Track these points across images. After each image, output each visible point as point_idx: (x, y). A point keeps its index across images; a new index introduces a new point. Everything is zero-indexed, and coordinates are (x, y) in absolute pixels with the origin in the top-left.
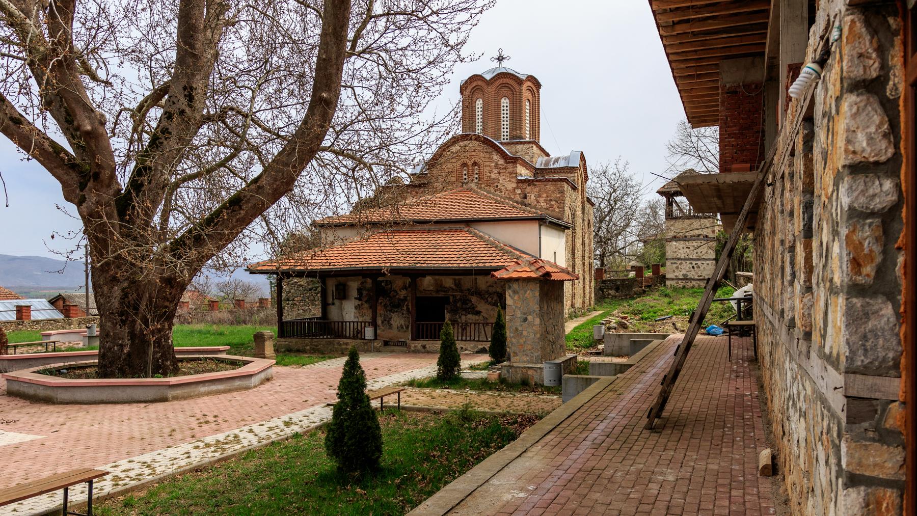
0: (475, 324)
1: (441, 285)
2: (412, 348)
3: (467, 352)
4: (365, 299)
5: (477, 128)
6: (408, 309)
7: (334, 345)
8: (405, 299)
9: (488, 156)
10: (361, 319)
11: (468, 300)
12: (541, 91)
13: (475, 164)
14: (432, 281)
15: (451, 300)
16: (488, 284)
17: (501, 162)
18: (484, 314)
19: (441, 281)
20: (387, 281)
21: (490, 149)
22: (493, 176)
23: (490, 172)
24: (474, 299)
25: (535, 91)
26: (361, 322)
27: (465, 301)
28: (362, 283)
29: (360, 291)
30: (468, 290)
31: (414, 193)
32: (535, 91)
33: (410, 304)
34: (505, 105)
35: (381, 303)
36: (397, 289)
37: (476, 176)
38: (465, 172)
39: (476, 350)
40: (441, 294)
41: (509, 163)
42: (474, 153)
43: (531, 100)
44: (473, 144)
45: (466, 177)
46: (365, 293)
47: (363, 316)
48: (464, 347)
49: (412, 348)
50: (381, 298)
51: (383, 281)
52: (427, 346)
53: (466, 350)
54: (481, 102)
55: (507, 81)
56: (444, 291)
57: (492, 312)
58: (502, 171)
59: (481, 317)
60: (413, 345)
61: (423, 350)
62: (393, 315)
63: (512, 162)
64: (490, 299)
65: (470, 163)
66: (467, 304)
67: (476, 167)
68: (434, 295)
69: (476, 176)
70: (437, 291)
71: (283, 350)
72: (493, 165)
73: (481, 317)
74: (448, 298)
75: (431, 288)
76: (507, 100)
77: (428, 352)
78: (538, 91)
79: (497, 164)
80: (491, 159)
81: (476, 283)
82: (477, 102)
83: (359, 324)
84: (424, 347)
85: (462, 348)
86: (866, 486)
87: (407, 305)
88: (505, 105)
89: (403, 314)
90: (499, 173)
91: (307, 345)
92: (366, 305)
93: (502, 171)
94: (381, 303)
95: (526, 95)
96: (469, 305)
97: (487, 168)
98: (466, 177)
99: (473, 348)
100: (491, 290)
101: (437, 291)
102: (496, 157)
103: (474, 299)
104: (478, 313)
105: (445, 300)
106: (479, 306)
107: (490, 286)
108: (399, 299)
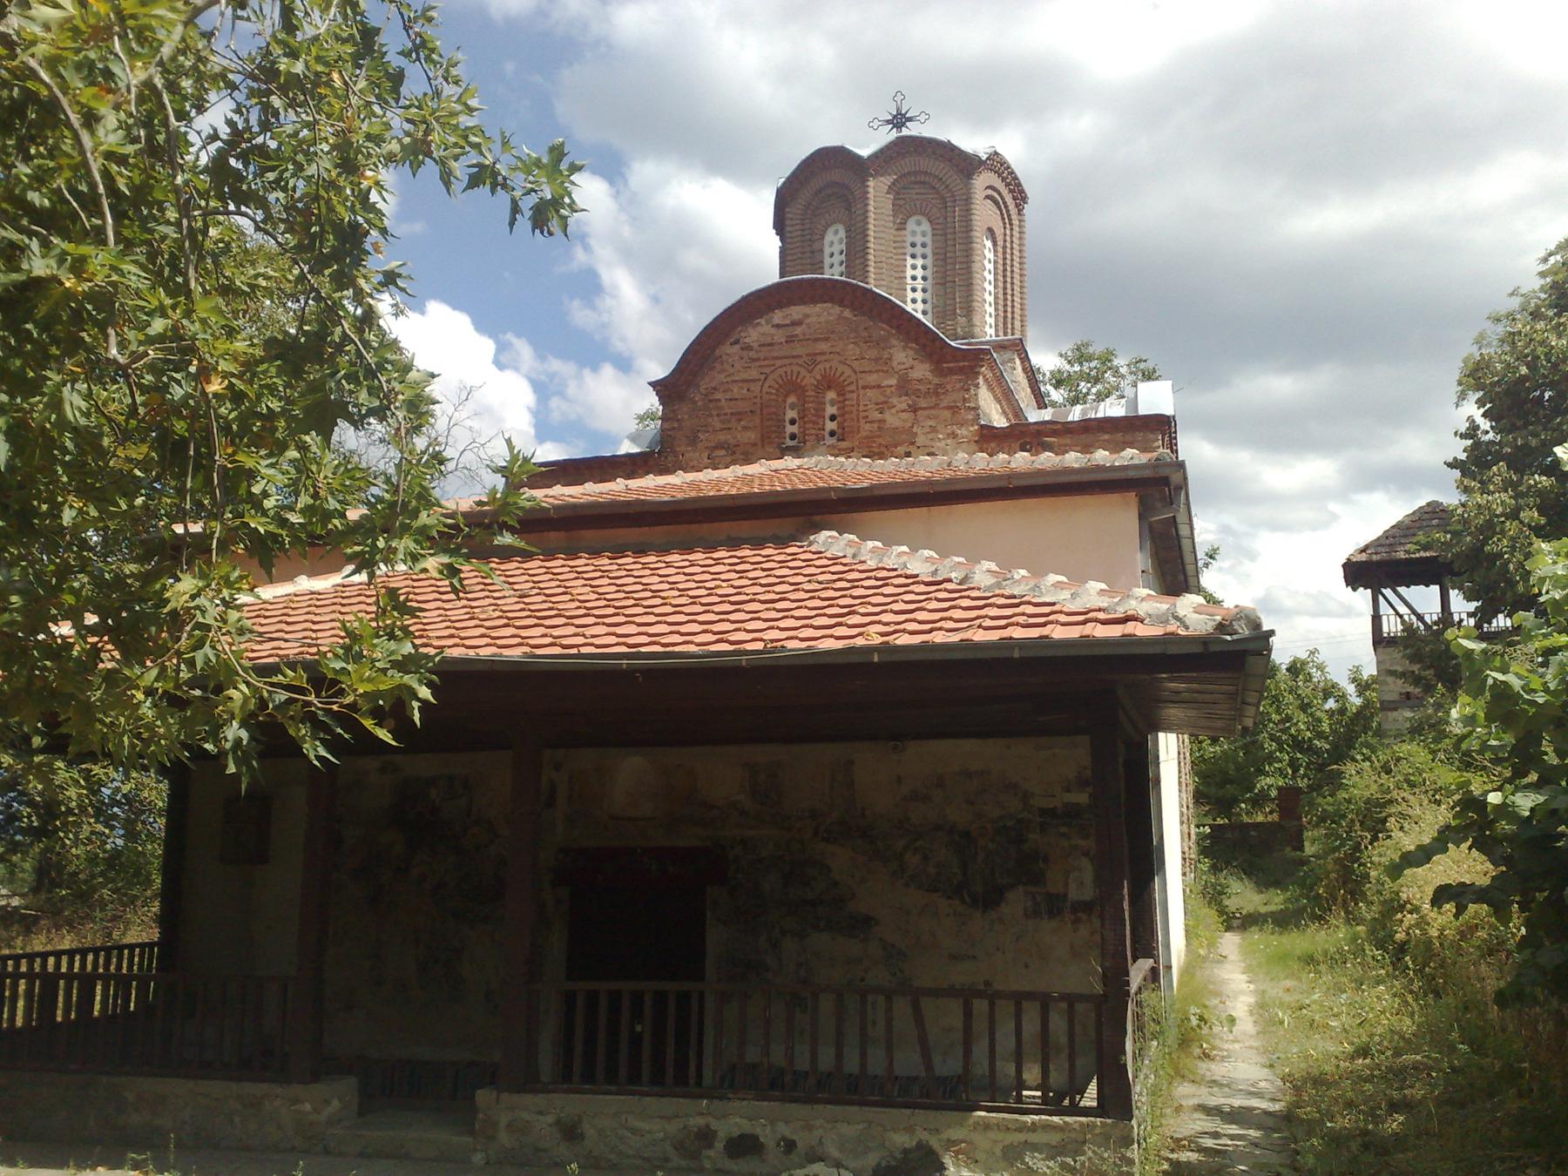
5: (827, 261)
9: (873, 353)
12: (1027, 209)
13: (829, 382)
17: (922, 372)
21: (882, 330)
22: (892, 419)
23: (883, 406)
25: (1012, 207)
32: (1012, 207)
34: (919, 240)
37: (830, 426)
38: (791, 414)
41: (951, 371)
42: (824, 346)
43: (999, 232)
44: (820, 314)
45: (794, 429)
48: (803, 1140)
49: (504, 1138)
52: (589, 1130)
54: (842, 234)
55: (926, 164)
58: (923, 403)
63: (961, 370)
65: (809, 380)
67: (831, 395)
69: (830, 426)
72: (893, 381)
76: (926, 226)
78: (1020, 212)
79: (904, 387)
80: (884, 365)
82: (830, 236)
84: (571, 1132)
85: (790, 1146)
86: (1013, 658)
88: (919, 240)
90: (914, 409)
93: (923, 403)
95: (984, 214)
97: (870, 393)
98: (794, 429)
102: (902, 356)
104: (861, 924)
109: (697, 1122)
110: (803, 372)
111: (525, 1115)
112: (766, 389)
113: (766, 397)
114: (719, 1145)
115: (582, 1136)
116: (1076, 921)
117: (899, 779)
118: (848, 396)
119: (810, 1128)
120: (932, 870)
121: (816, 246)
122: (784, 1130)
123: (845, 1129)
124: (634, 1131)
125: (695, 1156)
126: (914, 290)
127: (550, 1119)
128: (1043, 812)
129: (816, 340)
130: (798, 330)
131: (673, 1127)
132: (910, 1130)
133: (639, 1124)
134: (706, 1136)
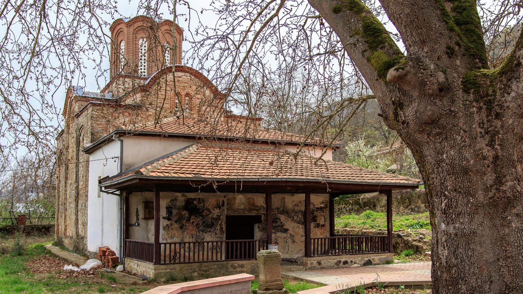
0: (180, 244)
1: (253, 204)
2: (309, 266)
3: (356, 265)
4: (175, 218)
6: (221, 228)
7: (227, 268)
8: (218, 218)
10: (169, 241)
11: (277, 218)
13: (187, 95)
14: (244, 200)
15: (262, 219)
16: (294, 203)
18: (290, 232)
19: (253, 199)
20: (199, 199)
24: (282, 218)
26: (170, 244)
27: (276, 220)
28: (172, 200)
29: (169, 209)
30: (278, 208)
31: (126, 114)
33: (223, 224)
35: (193, 222)
36: (210, 207)
39: (363, 262)
40: (254, 213)
46: (175, 212)
47: (172, 237)
48: (354, 261)
49: (309, 266)
50: (193, 217)
51: (195, 199)
52: (322, 262)
53: (355, 263)
56: (256, 210)
57: (297, 230)
59: (288, 234)
60: (309, 262)
61: (319, 267)
62: (206, 235)
64: (295, 218)
66: (276, 222)
68: (247, 214)
70: (250, 210)
71: (163, 280)
73: (288, 234)
74: (261, 216)
75: (242, 207)
77: (323, 268)
81: (284, 202)
83: (168, 245)
84: (319, 263)
85: (352, 261)
87: (221, 225)
89: (216, 234)
91: (194, 272)
92: (176, 226)
94: (193, 222)
96: (279, 223)
99: (361, 261)
100: (297, 208)
101: (250, 210)
103: (282, 218)
104: (286, 231)
105: (257, 219)
106: (286, 224)
107: (296, 205)
108: (212, 218)
109: (338, 259)
110: (182, 91)
111: (312, 261)
112: (171, 93)
113: (172, 96)
114: (342, 263)
115: (321, 264)
116: (322, 228)
117: (293, 201)
118: (193, 99)
119: (354, 259)
120: (299, 220)
121: (137, 42)
122: (351, 259)
123: (359, 258)
124: (330, 262)
125: (338, 265)
126: (145, 59)
127: (316, 261)
128: (317, 208)
129: (185, 83)
130: (180, 79)
131: (335, 261)
132: (367, 257)
133: (330, 261)
134: (340, 262)
